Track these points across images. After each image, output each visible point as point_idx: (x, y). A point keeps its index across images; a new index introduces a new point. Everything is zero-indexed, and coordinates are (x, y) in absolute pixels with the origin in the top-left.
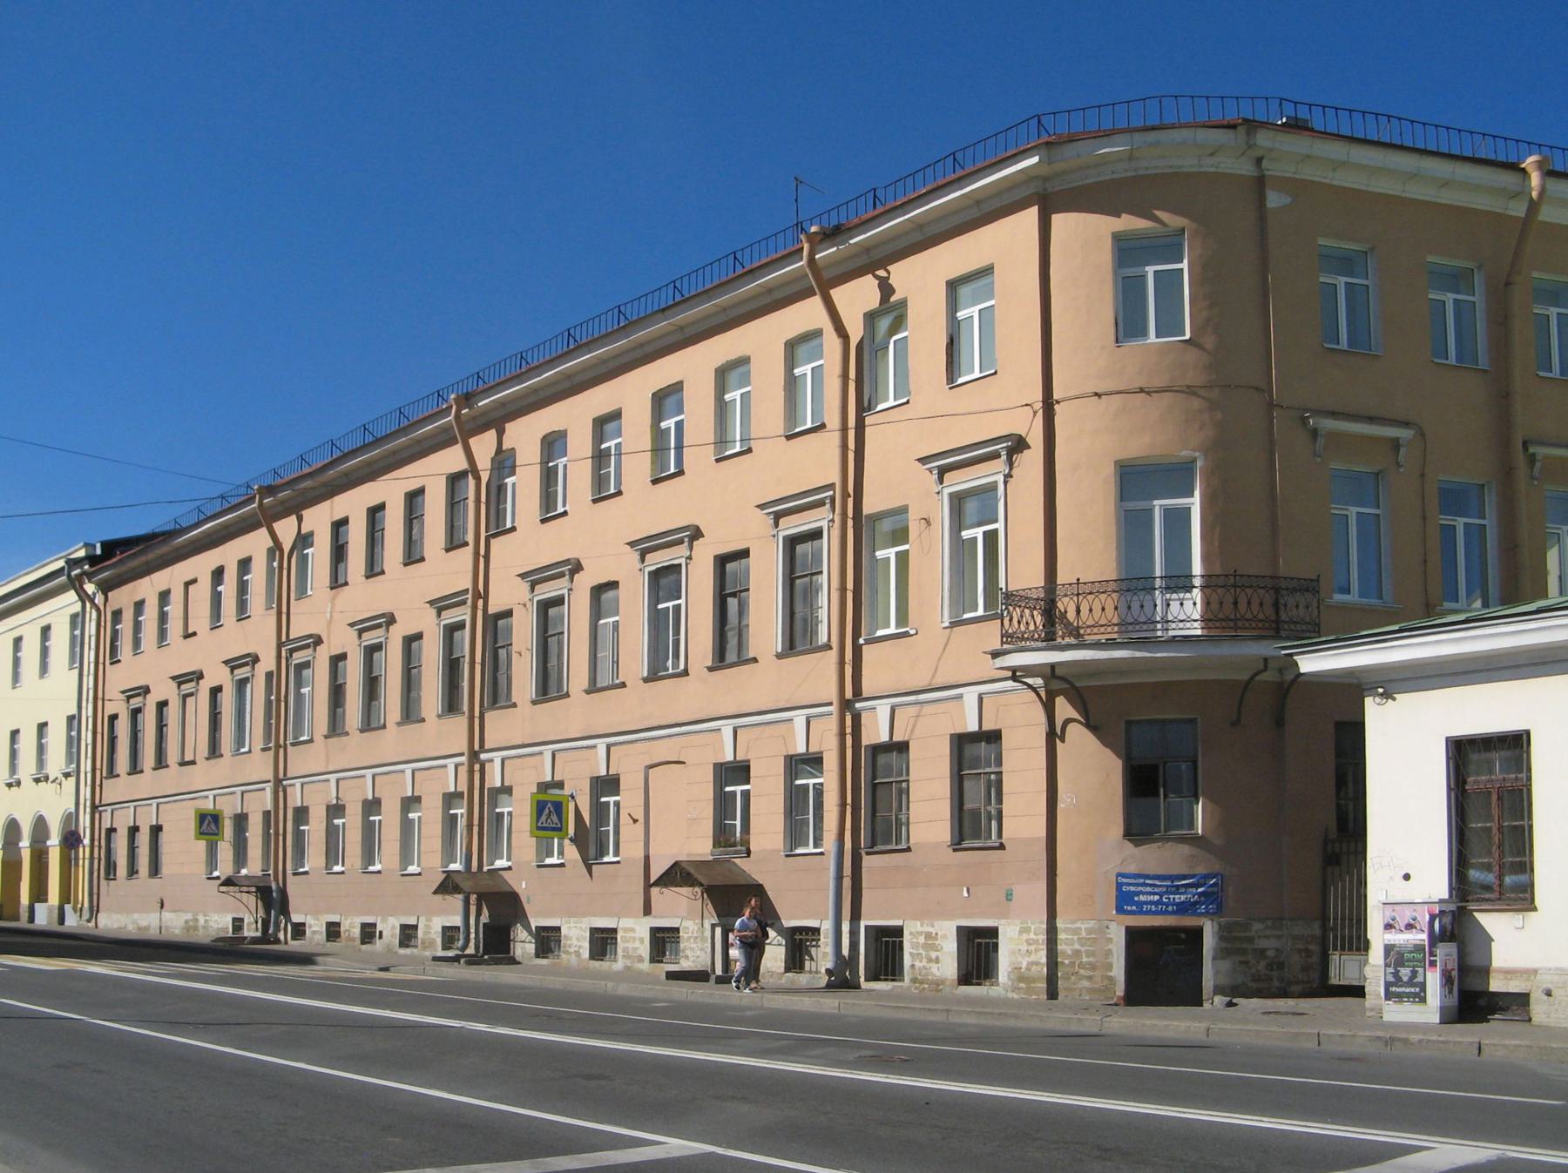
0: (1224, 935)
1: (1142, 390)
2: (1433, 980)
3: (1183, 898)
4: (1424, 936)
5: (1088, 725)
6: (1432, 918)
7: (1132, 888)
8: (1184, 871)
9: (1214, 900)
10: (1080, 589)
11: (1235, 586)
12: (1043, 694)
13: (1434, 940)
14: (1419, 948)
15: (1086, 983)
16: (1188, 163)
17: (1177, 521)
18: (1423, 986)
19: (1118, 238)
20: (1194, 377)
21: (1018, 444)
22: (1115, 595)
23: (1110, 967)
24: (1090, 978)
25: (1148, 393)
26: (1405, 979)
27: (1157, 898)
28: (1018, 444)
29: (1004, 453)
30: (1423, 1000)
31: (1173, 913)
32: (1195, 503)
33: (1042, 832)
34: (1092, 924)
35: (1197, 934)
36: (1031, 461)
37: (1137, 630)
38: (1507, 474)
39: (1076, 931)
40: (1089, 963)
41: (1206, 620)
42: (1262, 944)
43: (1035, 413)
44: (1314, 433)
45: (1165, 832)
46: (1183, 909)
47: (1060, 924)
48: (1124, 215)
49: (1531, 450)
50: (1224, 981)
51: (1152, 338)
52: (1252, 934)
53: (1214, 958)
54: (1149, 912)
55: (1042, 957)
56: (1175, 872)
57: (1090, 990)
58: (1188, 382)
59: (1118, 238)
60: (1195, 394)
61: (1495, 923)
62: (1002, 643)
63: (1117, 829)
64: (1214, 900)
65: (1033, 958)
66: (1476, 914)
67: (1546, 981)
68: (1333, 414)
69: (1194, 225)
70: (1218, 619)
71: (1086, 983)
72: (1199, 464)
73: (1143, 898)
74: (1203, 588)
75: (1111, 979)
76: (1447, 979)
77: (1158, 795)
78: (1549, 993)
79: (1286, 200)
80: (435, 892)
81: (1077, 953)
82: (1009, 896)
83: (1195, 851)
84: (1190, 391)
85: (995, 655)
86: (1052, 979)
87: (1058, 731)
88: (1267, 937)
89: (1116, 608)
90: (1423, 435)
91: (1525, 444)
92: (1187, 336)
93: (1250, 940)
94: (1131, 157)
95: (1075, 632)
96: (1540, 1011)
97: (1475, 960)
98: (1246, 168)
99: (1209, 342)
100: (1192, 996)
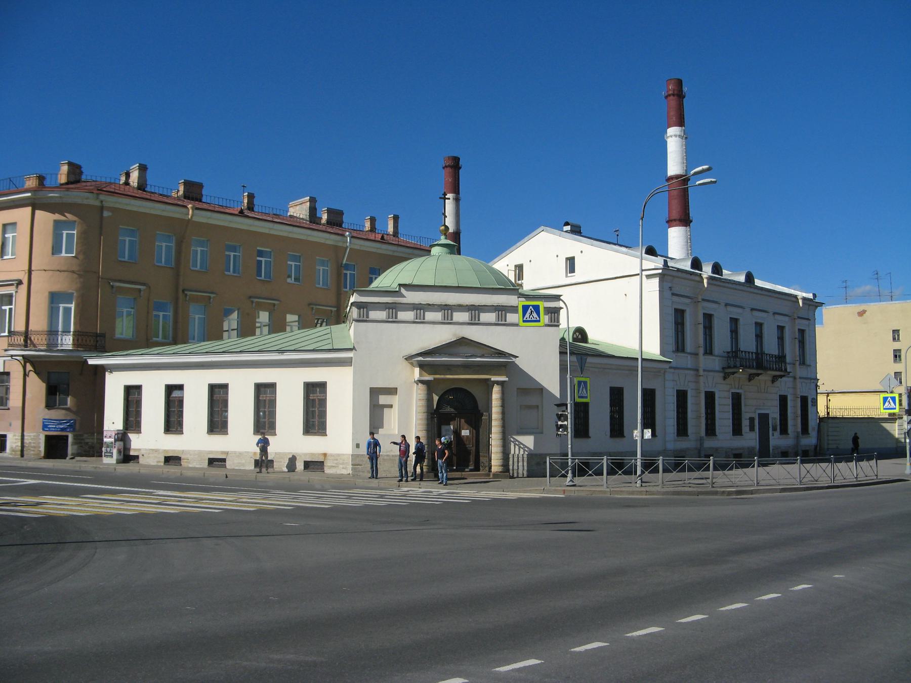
0: (76, 438)
1: (58, 270)
2: (115, 452)
3: (63, 426)
4: (113, 440)
5: (35, 372)
6: (115, 434)
7: (47, 423)
8: (63, 419)
9: (72, 427)
10: (38, 333)
11: (78, 335)
12: (23, 363)
13: (116, 441)
14: (112, 443)
15: (32, 452)
16: (79, 201)
17: (67, 311)
18: (112, 453)
19: (55, 221)
20: (75, 268)
21: (20, 282)
22: (46, 336)
23: (40, 447)
24: (33, 450)
25: (60, 271)
26: (109, 451)
27: (54, 426)
28: (20, 282)
29: (15, 285)
30: (112, 457)
31: (59, 431)
32: (73, 306)
33: (20, 405)
34: (35, 434)
35: (67, 437)
36: (24, 288)
37: (52, 346)
38: (176, 300)
39: (30, 436)
40: (34, 446)
41: (74, 344)
42: (87, 441)
43: (26, 273)
44: (112, 287)
45: (59, 405)
46: (63, 430)
47: (25, 434)
48: (56, 214)
49: (186, 292)
50: (75, 452)
51: (64, 254)
52: (83, 438)
53: (72, 445)
54: (52, 431)
55: (19, 444)
56: (60, 418)
57: (34, 454)
58: (73, 269)
59: (55, 221)
60: (75, 273)
61: (132, 436)
62: (8, 347)
63: (43, 404)
64: (72, 427)
65: (17, 445)
66: (129, 434)
67: (143, 452)
68: (120, 281)
69: (80, 220)
70: (76, 343)
71: (32, 452)
72: (75, 294)
73: (51, 426)
74: (73, 335)
75: (40, 451)
76: (119, 452)
77: (57, 395)
78: (143, 456)
79: (110, 214)
80: (856, 434)
81: (30, 443)
82: (10, 425)
83: (67, 412)
84: (73, 272)
85: (6, 350)
86: (22, 451)
87: (27, 374)
88: (89, 439)
89: (46, 339)
90: (150, 287)
91: (183, 291)
92: (74, 255)
93: (83, 439)
94: (60, 197)
95: (35, 346)
96: (229, 464)
97: (128, 447)
98: (97, 203)
99: (81, 257)
100: (63, 455)
